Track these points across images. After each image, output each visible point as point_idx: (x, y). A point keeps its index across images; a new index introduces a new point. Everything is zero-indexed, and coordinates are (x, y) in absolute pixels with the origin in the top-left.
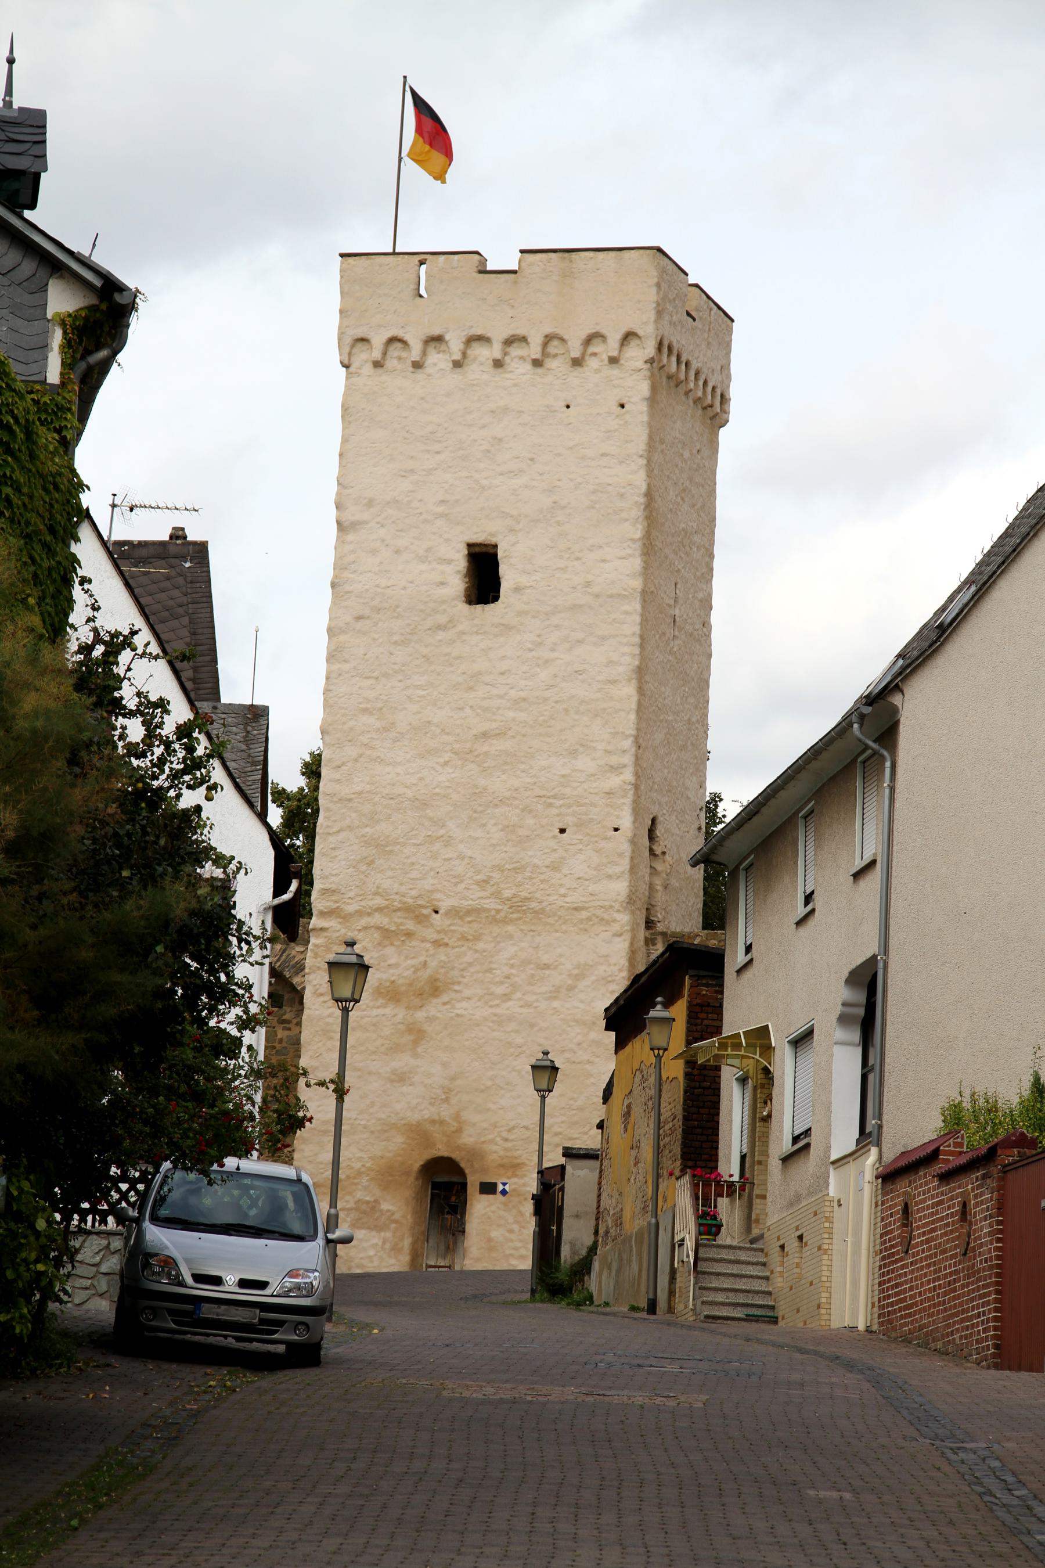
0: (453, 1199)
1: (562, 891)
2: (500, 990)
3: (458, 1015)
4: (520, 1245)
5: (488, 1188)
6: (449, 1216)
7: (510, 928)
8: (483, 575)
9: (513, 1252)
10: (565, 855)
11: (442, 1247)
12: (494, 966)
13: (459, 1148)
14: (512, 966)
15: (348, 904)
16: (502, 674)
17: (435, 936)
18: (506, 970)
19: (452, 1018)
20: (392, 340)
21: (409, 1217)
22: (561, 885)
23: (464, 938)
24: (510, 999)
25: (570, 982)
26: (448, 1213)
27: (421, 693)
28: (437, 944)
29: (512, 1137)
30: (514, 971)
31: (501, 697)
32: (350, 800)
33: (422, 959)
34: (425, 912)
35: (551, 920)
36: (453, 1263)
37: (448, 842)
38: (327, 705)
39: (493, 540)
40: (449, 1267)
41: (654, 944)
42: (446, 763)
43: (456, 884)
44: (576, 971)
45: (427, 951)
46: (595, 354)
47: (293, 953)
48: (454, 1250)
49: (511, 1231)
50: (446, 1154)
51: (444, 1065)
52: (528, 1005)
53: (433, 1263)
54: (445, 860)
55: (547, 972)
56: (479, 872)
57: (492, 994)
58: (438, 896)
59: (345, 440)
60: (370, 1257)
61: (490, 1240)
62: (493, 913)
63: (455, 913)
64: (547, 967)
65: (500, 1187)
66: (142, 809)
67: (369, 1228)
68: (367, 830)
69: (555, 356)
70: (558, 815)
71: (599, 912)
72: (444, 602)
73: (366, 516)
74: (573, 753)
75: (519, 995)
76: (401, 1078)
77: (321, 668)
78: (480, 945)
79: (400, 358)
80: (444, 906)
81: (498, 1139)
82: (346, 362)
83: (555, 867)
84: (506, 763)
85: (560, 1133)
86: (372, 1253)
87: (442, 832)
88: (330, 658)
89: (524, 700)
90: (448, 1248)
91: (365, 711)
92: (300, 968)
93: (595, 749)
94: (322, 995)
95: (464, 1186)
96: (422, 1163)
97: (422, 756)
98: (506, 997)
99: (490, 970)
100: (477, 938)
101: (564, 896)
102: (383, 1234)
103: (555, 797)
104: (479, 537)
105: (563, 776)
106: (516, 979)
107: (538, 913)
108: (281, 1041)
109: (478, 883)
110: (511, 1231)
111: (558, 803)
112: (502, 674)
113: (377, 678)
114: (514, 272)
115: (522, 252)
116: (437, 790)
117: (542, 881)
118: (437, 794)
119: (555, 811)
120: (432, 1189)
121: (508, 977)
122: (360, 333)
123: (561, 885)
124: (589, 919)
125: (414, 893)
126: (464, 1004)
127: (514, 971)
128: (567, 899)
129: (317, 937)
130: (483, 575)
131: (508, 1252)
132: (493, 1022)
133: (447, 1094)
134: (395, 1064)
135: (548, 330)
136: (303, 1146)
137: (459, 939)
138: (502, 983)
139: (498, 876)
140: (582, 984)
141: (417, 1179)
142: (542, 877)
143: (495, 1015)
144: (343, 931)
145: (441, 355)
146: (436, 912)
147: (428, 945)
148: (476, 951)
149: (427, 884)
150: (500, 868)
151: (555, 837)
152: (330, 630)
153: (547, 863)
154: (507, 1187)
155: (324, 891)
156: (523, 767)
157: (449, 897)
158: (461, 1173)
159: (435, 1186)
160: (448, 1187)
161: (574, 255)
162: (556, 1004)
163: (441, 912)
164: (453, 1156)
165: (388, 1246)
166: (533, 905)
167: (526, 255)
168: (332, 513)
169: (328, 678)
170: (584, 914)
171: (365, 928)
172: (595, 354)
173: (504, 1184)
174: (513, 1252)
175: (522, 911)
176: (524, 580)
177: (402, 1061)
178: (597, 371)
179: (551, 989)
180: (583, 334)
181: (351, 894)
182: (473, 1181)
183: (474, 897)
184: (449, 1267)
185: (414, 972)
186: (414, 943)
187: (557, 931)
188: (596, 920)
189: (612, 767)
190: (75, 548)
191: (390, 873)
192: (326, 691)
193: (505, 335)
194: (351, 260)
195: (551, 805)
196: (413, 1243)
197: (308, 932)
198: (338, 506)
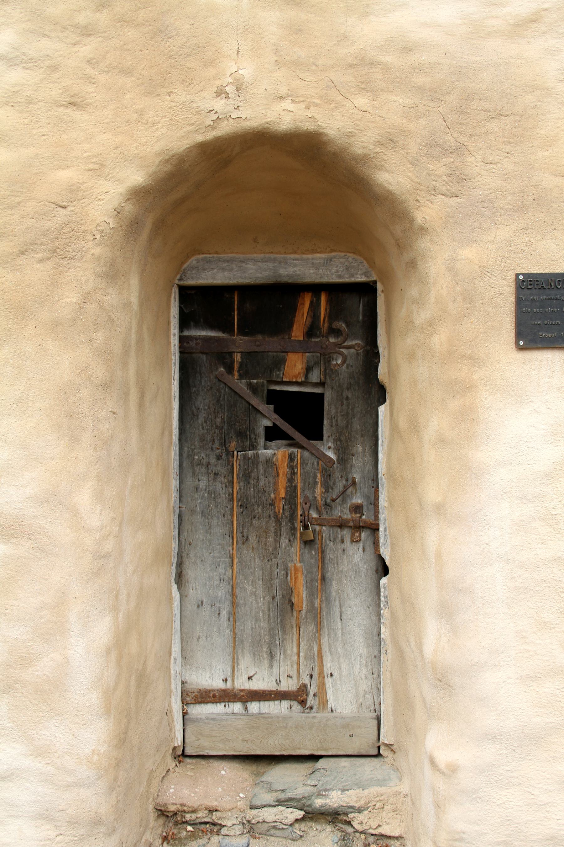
0: (295, 365)
6: (277, 452)
11: (256, 600)
13: (366, 72)
21: (84, 499)
26: (273, 434)
36: (319, 674)
40: (299, 696)
48: (317, 617)
50: (285, 116)
53: (215, 682)
90: (285, 607)
96: (137, 177)
120: (184, 323)
141: (112, 274)
159: (200, 305)
164: (334, 123)
184: (299, 696)
190: (272, 407)
196: (119, 645)
197: (286, 499)
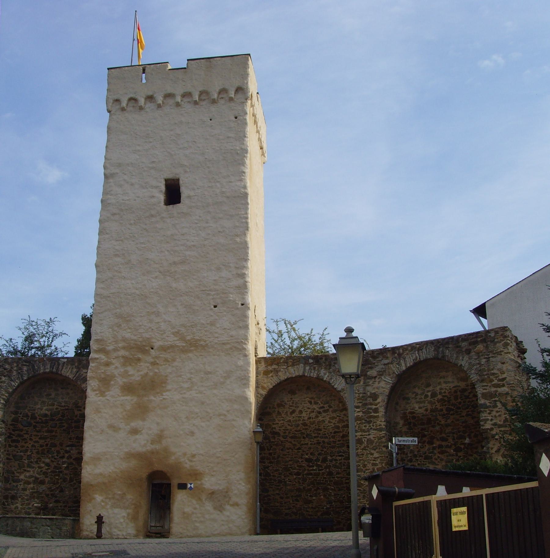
1: (216, 335)
2: (186, 385)
3: (164, 399)
4: (200, 515)
5: (182, 486)
7: (190, 355)
8: (173, 193)
9: (197, 519)
10: (217, 318)
12: (183, 374)
14: (191, 373)
15: (109, 346)
16: (183, 235)
17: (152, 360)
18: (189, 375)
19: (161, 400)
20: (131, 99)
22: (216, 333)
23: (166, 360)
24: (191, 390)
25: (222, 380)
27: (143, 246)
28: (154, 364)
29: (194, 460)
30: (192, 376)
31: (182, 245)
32: (109, 297)
33: (145, 371)
34: (147, 348)
35: (211, 350)
37: (158, 314)
38: (98, 254)
39: (177, 176)
41: (260, 363)
42: (156, 277)
43: (162, 334)
44: (225, 375)
45: (148, 367)
46: (222, 98)
47: (82, 373)
49: (195, 509)
50: (160, 469)
51: (158, 424)
52: (201, 392)
53: (153, 525)
54: (156, 323)
55: (210, 376)
56: (174, 328)
57: (181, 387)
58: (154, 340)
59: (108, 141)
60: (121, 523)
61: (184, 513)
62: (181, 348)
63: (163, 349)
64: (210, 373)
65: (189, 486)
66: (519, 458)
67: (120, 508)
68: (118, 310)
69: (205, 100)
70: (213, 299)
71: (236, 345)
72: (155, 204)
73: (117, 171)
74: (219, 269)
75: (196, 388)
76: (135, 431)
77: (95, 238)
78: (176, 364)
79: (133, 107)
80: (157, 344)
81: (187, 461)
82: (110, 109)
83: (212, 324)
84: (186, 276)
85: (220, 457)
86: (122, 520)
87: (155, 309)
88: (101, 233)
89: (194, 246)
91: (116, 255)
92: (85, 380)
93: (230, 267)
94: (95, 390)
95: (169, 485)
97: (144, 275)
98: (189, 389)
99: (180, 376)
100: (174, 360)
101: (217, 338)
102: (127, 510)
103: (210, 290)
104: (170, 176)
105: (215, 280)
106: (194, 380)
107: (203, 347)
108: (76, 416)
109: (173, 334)
110: (195, 509)
111: (213, 293)
112: (183, 235)
113: (122, 240)
114: (185, 68)
115: (188, 60)
116: (152, 290)
117: (206, 331)
118: (152, 292)
119: (211, 297)
121: (190, 379)
122: (116, 97)
123: (216, 333)
124: (231, 348)
125: (141, 339)
126: (167, 393)
127: (192, 376)
128: (219, 339)
129: (93, 363)
130: (173, 193)
131: (194, 519)
132: (182, 401)
133: (160, 437)
134: (133, 424)
135: (201, 89)
136: (87, 466)
137: (164, 361)
138: (187, 382)
139: (183, 330)
140: (228, 382)
142: (206, 329)
143: (183, 398)
144: (106, 359)
145: (152, 104)
146: (152, 349)
147: (148, 365)
148: (173, 367)
149: (146, 335)
150: (183, 325)
151: (211, 309)
152: (100, 221)
153: (208, 322)
154: (192, 486)
155: (97, 341)
156: (195, 277)
157: (158, 340)
158: (168, 479)
159: (154, 485)
160: (161, 485)
161: (211, 60)
162: (215, 391)
163: (155, 348)
165: (130, 517)
166: (202, 343)
167: (190, 61)
168: (102, 171)
169: (99, 242)
170: (228, 346)
171: (116, 357)
172: (222, 98)
173: (191, 484)
174: (197, 519)
175: (194, 346)
176: (192, 193)
177: (136, 424)
178: (223, 105)
179: (212, 384)
180: (218, 89)
181: (110, 341)
182: (175, 482)
183: (172, 340)
184: (162, 527)
185: (142, 378)
186: (142, 364)
187: (214, 355)
188: (234, 349)
189: (239, 275)
191: (129, 331)
192: (98, 248)
193: (182, 92)
194: (112, 70)
195: (209, 294)
198: (105, 167)
